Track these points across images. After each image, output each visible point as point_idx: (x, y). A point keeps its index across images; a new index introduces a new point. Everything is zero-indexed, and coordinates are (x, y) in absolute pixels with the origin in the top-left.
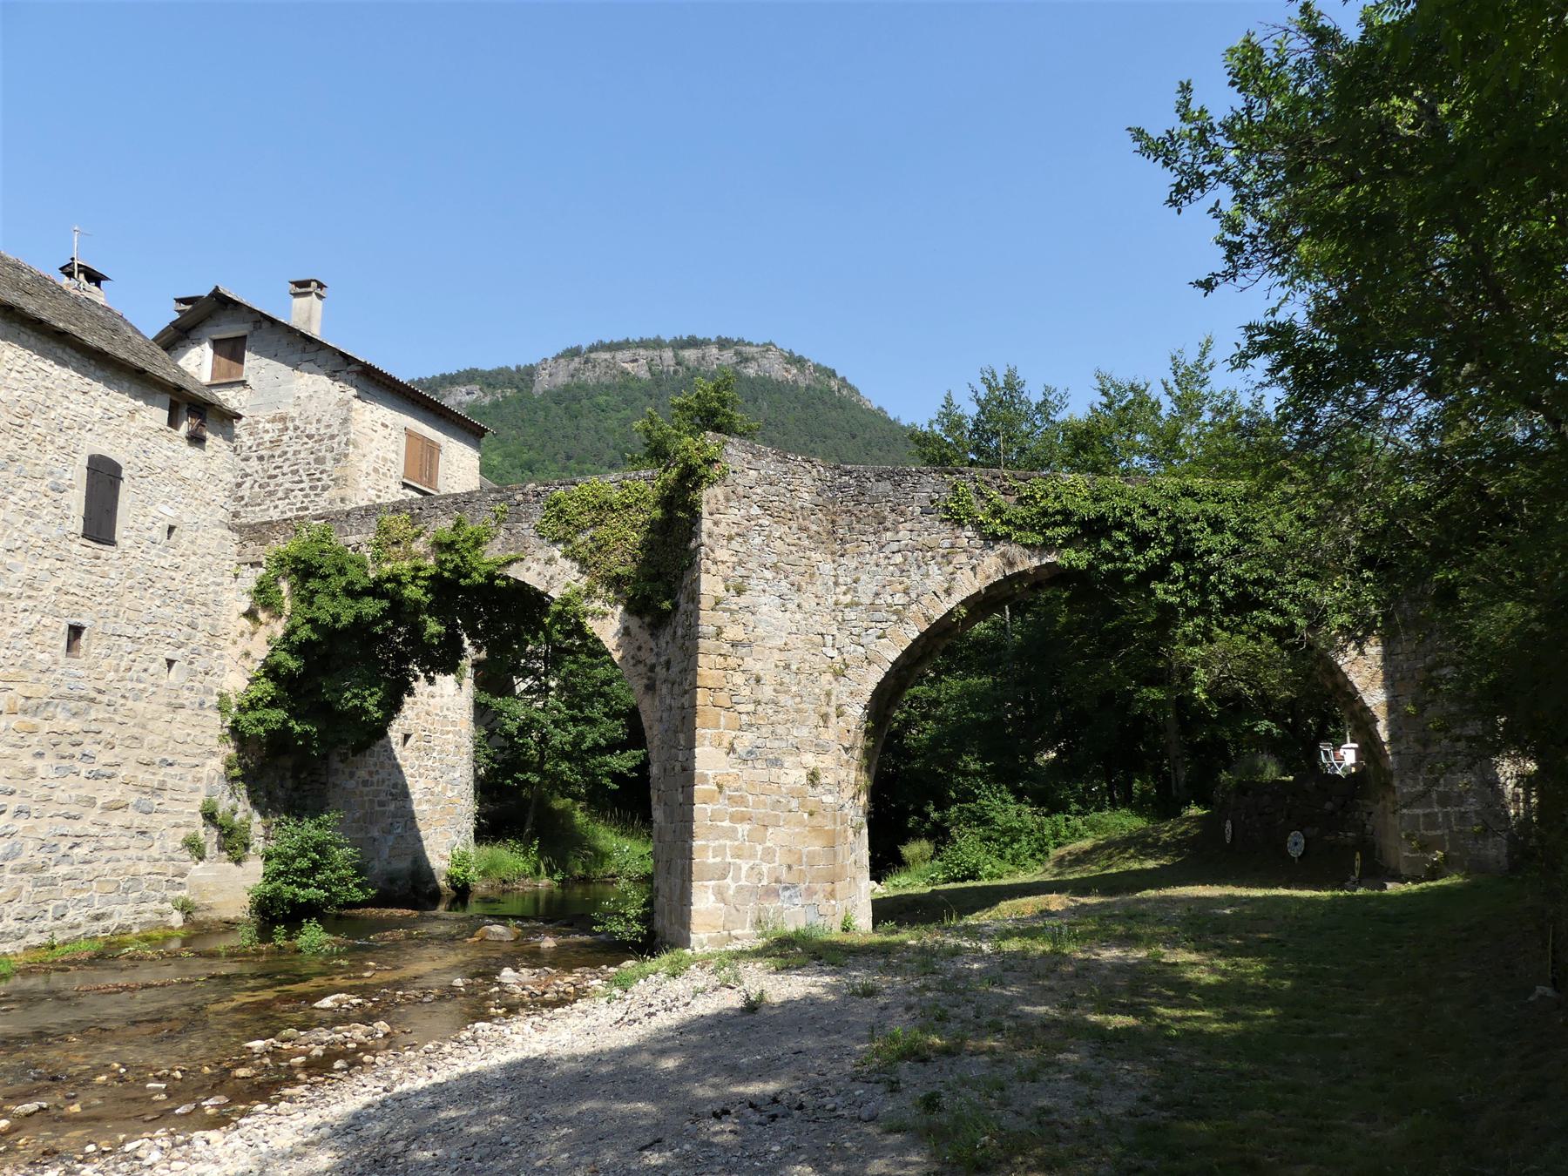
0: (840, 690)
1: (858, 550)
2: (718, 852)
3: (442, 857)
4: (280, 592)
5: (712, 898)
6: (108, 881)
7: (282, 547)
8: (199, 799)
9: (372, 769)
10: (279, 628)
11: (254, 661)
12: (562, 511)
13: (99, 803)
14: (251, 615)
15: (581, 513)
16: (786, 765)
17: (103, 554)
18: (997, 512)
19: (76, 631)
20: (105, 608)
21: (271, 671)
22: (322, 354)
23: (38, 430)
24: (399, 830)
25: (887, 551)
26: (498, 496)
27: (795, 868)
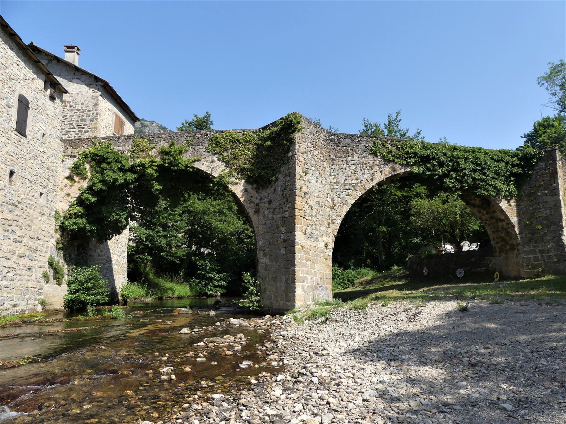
0: (333, 213)
1: (338, 163)
2: (303, 272)
3: (120, 287)
4: (85, 169)
5: (301, 290)
6: (19, 289)
7: (86, 150)
8: (48, 256)
9: (101, 249)
10: (85, 184)
11: (72, 198)
12: (218, 142)
13: (17, 254)
14: (70, 178)
15: (226, 143)
16: (319, 240)
17: (22, 140)
18: (390, 152)
19: (12, 173)
20: (22, 165)
21: (80, 201)
22: (84, 77)
23: (3, 76)
24: (108, 276)
25: (350, 164)
26: (189, 135)
27: (322, 279)
